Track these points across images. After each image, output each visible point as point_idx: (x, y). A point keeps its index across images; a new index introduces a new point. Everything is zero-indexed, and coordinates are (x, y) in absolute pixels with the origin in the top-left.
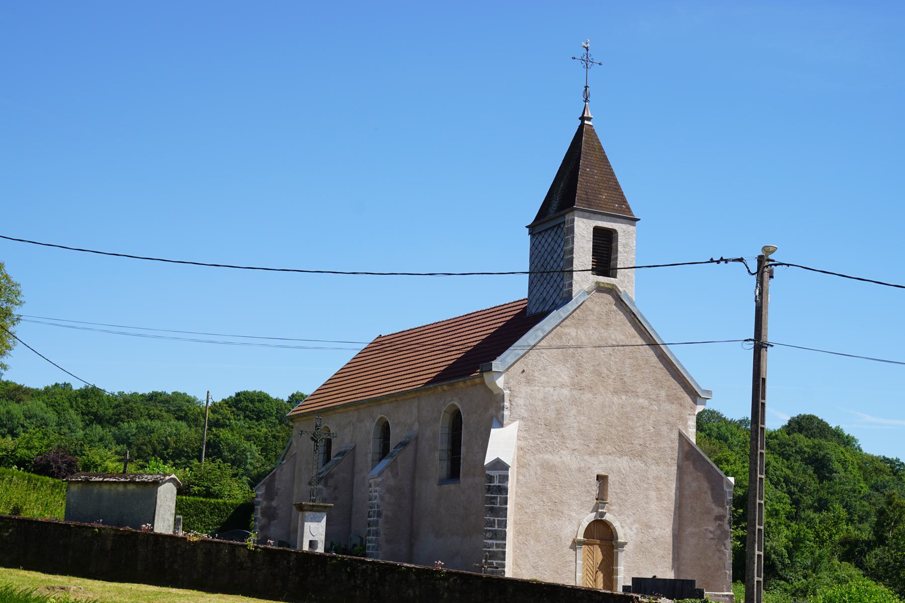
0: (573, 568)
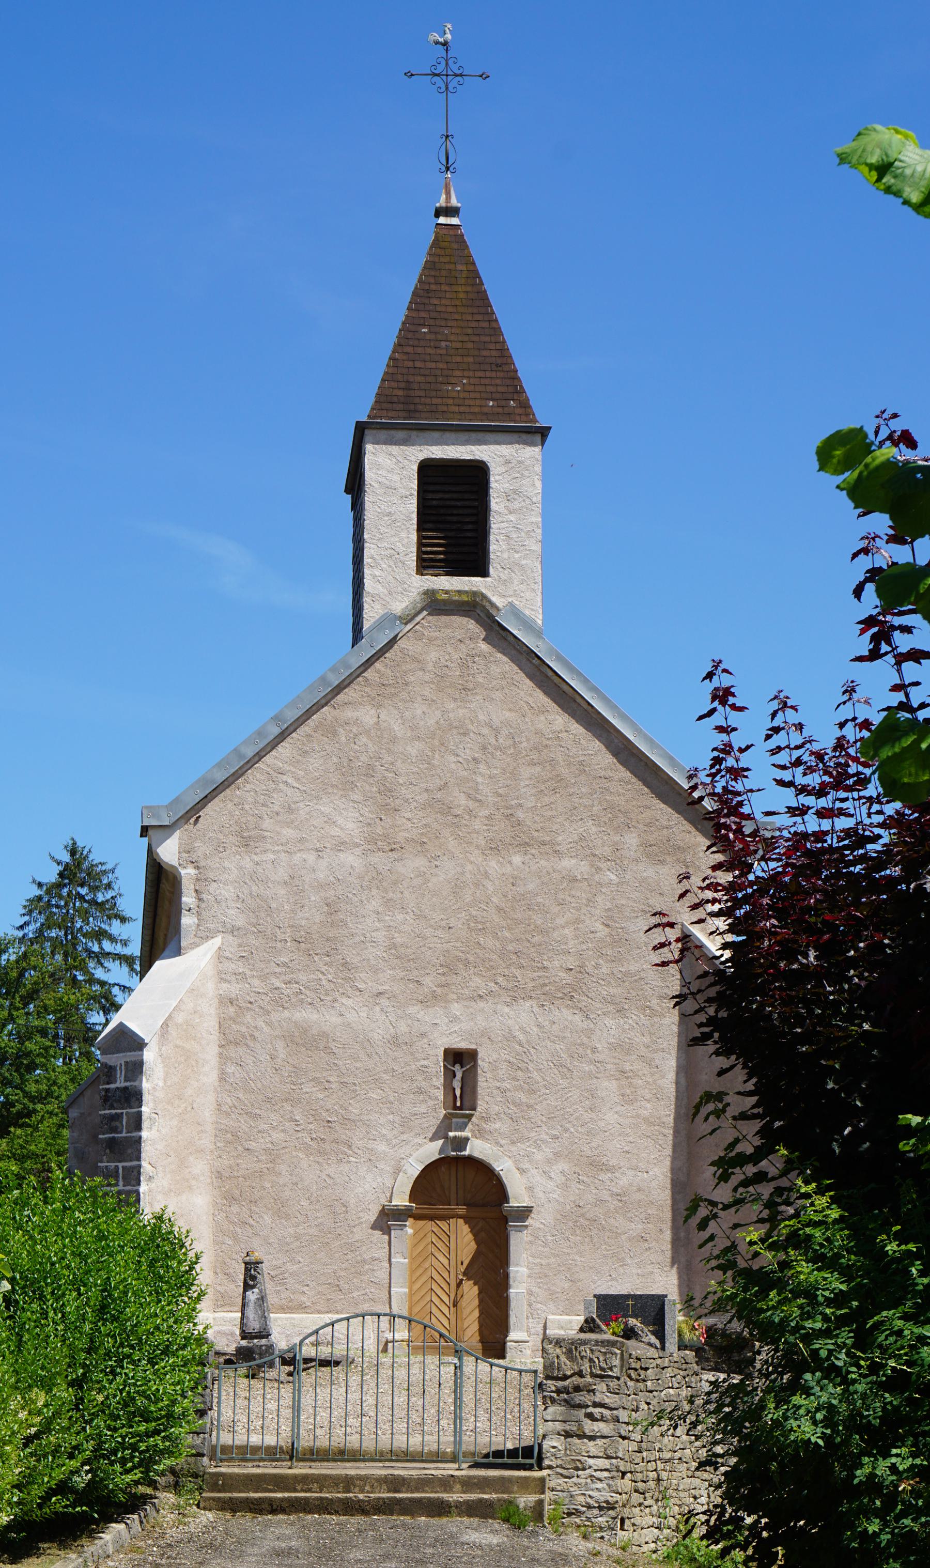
0: (382, 1275)
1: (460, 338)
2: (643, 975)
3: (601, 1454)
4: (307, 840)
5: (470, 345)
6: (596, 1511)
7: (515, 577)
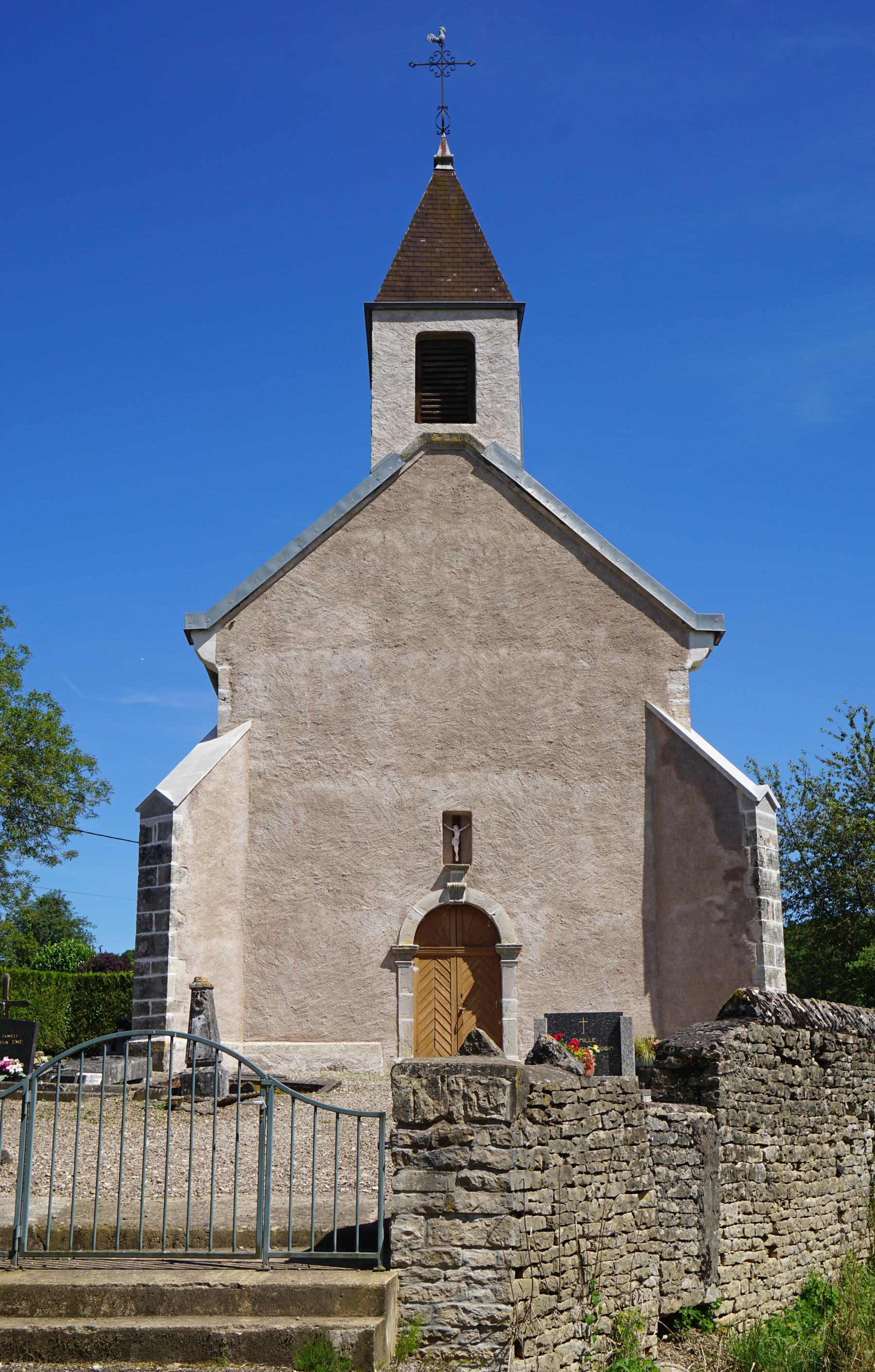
0: (391, 1007)
1: (452, 245)
2: (613, 745)
3: (482, 1243)
4: (325, 640)
5: (459, 250)
6: (474, 1334)
7: (499, 421)
